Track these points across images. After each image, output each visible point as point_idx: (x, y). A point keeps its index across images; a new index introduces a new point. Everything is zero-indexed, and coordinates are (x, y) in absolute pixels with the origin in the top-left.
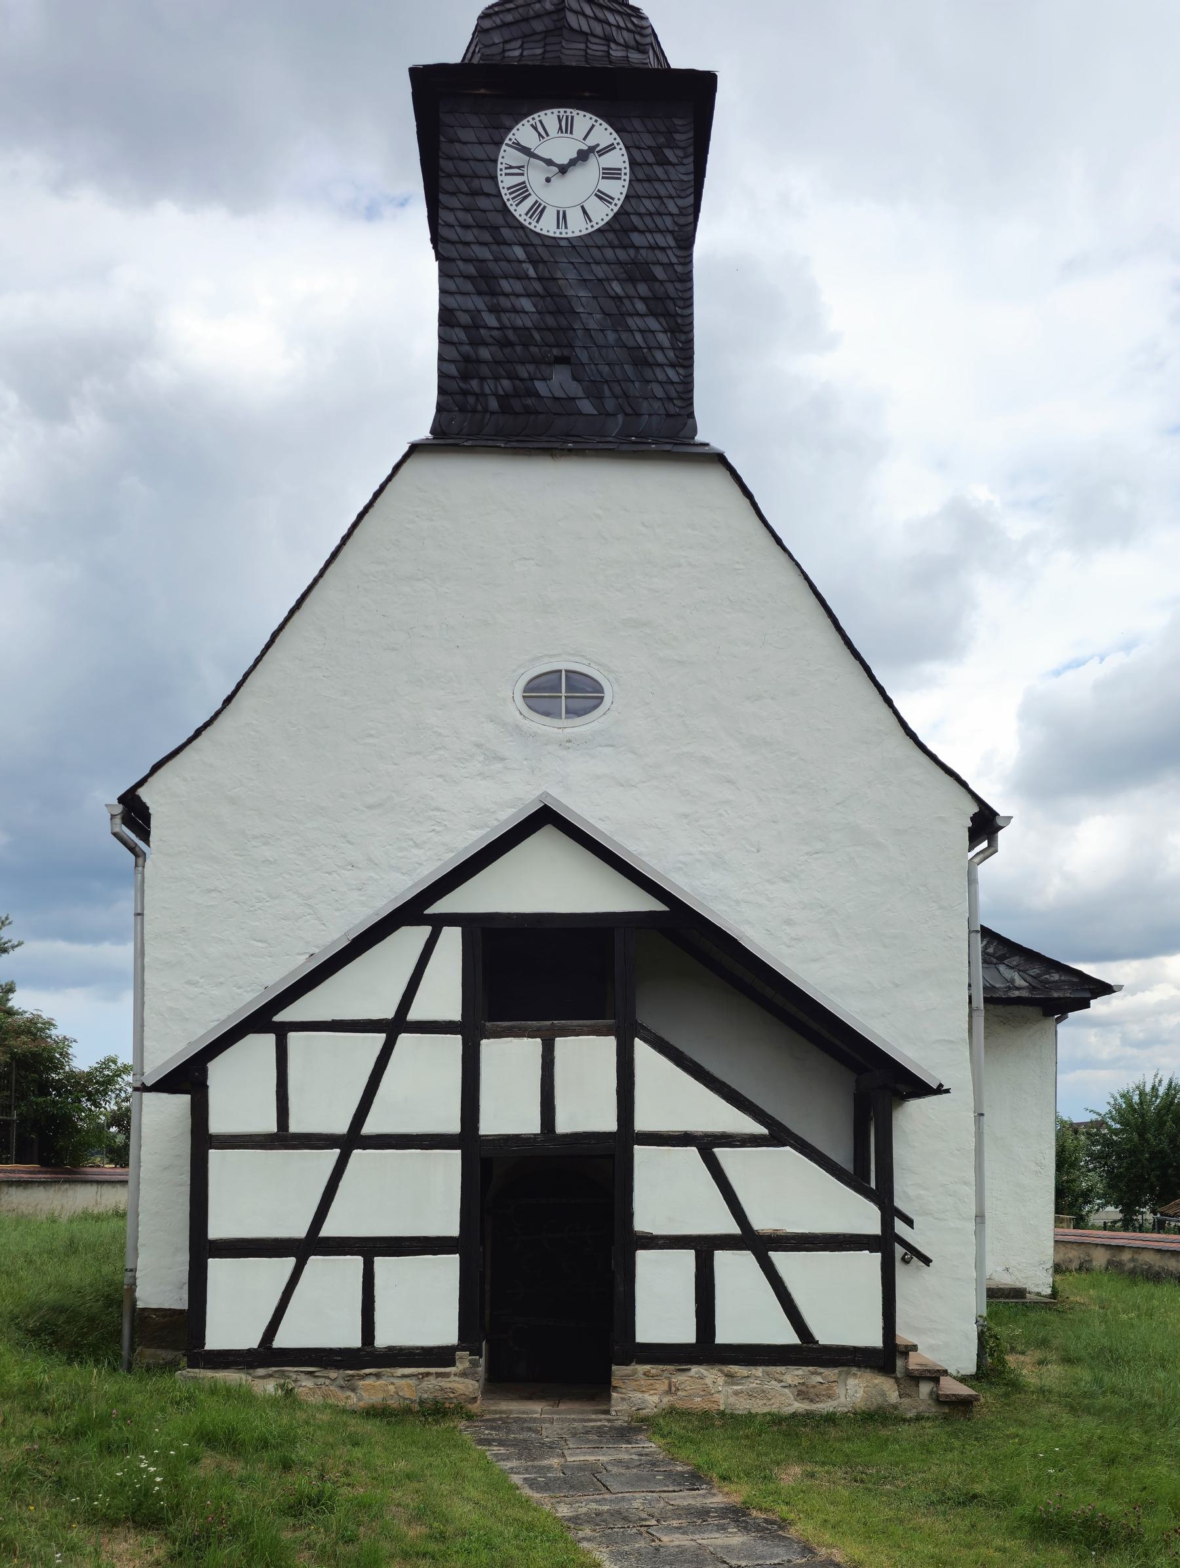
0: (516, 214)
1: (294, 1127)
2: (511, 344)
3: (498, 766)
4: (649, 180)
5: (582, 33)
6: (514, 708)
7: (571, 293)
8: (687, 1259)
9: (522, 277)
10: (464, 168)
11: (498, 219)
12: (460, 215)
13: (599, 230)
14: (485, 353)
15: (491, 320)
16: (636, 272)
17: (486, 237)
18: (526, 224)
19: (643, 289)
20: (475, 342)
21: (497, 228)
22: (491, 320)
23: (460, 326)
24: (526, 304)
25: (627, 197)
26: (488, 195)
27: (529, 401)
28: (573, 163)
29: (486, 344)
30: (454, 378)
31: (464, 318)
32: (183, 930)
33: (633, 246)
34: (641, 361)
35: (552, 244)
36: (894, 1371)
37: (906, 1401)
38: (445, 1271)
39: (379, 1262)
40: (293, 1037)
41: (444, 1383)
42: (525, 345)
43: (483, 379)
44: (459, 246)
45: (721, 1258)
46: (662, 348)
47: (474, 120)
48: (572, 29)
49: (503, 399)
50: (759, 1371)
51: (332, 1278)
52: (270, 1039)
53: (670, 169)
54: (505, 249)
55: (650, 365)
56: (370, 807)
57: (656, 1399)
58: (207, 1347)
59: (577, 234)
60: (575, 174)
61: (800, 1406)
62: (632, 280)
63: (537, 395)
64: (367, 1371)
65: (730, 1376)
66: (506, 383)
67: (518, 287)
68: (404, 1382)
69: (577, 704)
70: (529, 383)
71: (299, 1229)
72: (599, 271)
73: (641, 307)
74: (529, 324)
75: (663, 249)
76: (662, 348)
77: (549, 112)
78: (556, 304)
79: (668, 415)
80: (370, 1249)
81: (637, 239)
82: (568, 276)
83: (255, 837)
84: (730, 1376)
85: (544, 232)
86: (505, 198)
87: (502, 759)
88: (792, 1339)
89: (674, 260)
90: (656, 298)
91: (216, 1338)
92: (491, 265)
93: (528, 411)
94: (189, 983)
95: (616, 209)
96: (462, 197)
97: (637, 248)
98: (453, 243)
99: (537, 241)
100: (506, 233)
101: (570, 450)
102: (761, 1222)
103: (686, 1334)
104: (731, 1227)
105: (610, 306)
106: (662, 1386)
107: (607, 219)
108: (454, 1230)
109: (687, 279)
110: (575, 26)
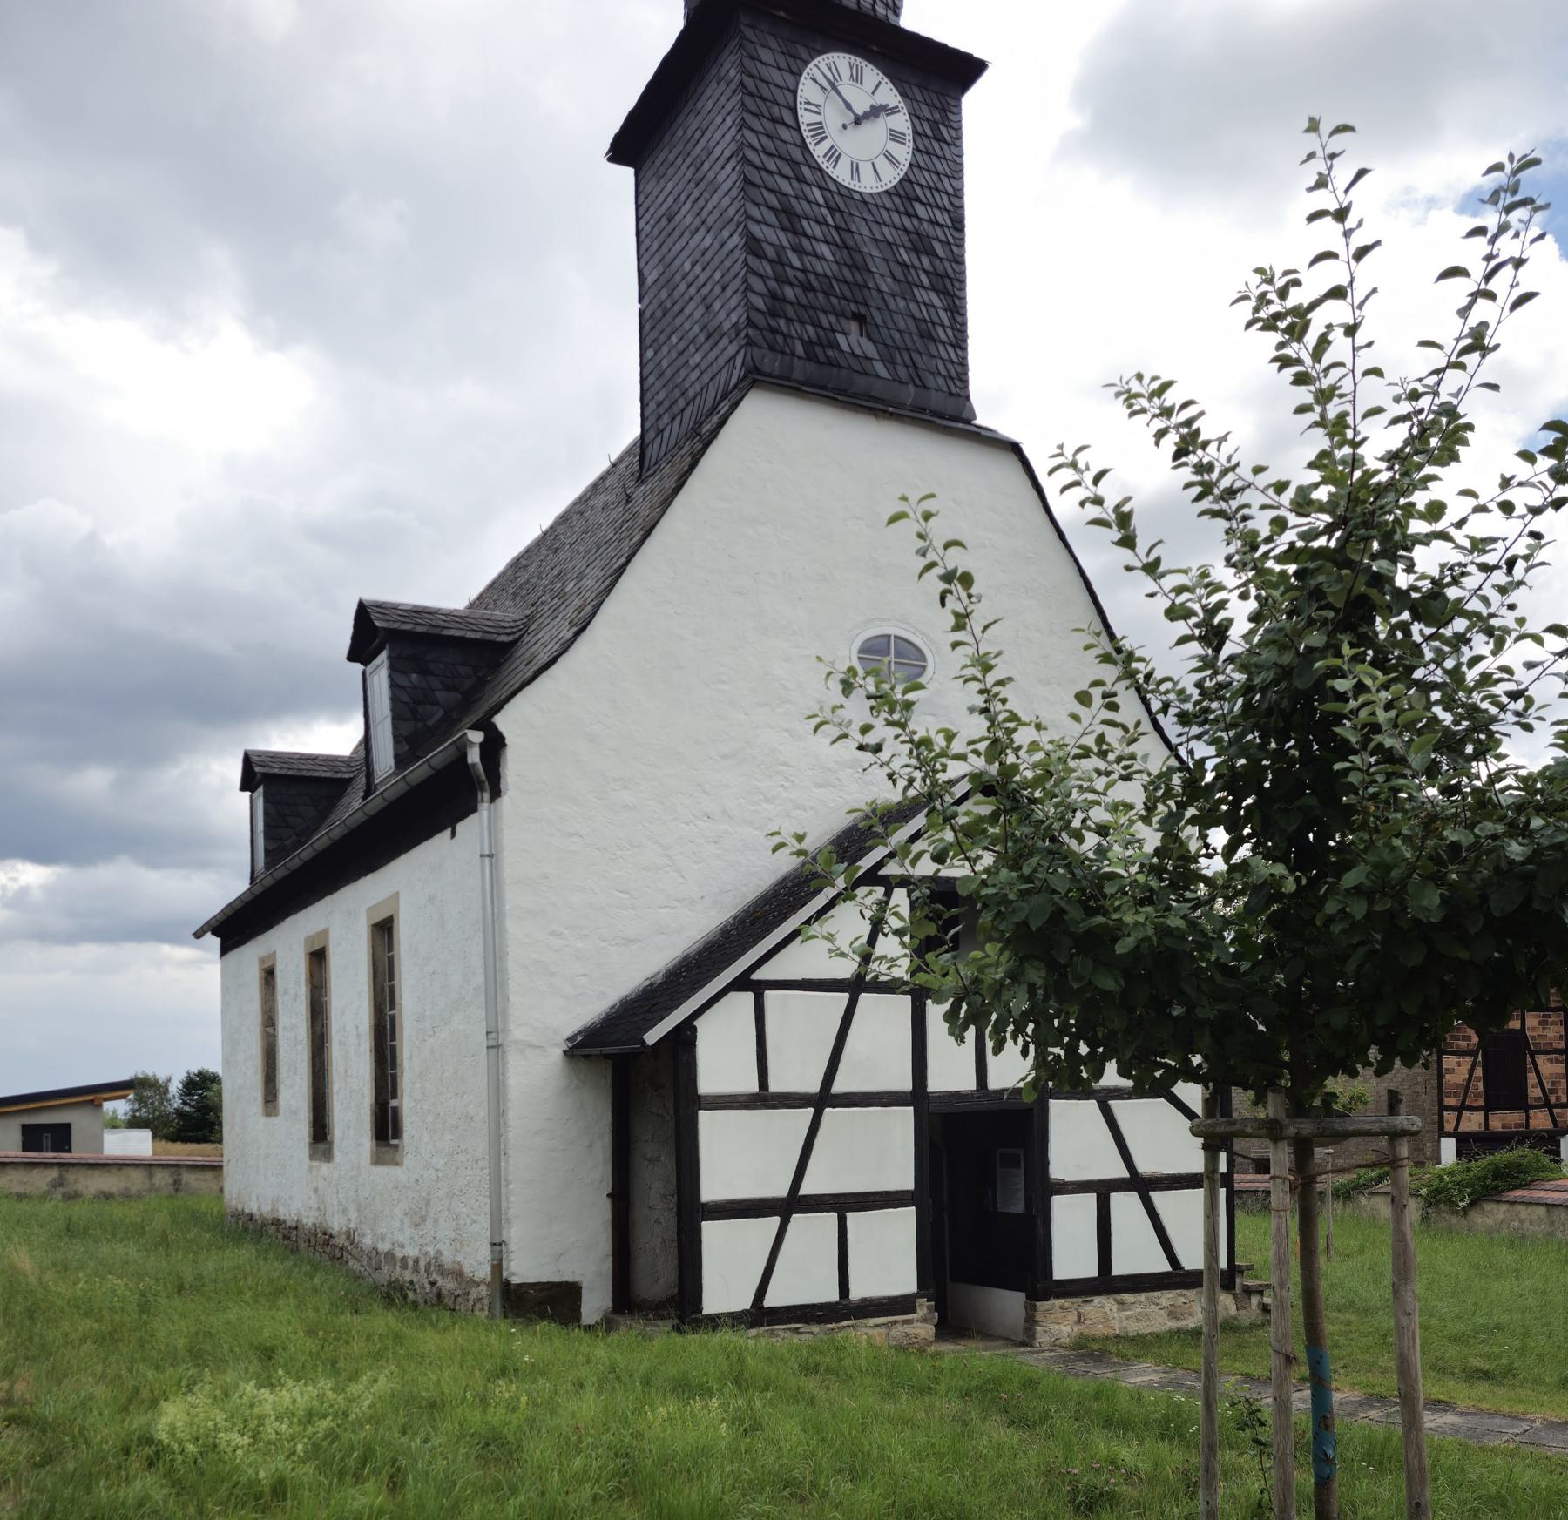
0: (815, 154)
1: (774, 1087)
2: (813, 290)
7: (865, 250)
8: (1091, 1199)
9: (822, 222)
11: (797, 154)
12: (764, 139)
13: (887, 192)
14: (789, 293)
15: (795, 260)
17: (787, 170)
19: (925, 261)
21: (798, 164)
22: (795, 260)
24: (824, 250)
26: (788, 126)
27: (830, 353)
28: (867, 116)
29: (791, 285)
31: (770, 252)
35: (847, 194)
36: (577, 1317)
37: (1242, 1312)
39: (851, 1217)
40: (770, 996)
41: (908, 1329)
42: (826, 294)
44: (764, 174)
45: (1116, 1199)
46: (943, 326)
47: (772, 43)
49: (808, 344)
50: (1142, 1297)
52: (749, 997)
54: (806, 188)
55: (934, 340)
56: (725, 757)
57: (1068, 1329)
58: (705, 1312)
59: (868, 190)
61: (1173, 1324)
62: (916, 250)
63: (840, 350)
64: (845, 1323)
65: (1121, 1303)
66: (810, 329)
67: (818, 232)
68: (876, 1331)
70: (830, 334)
74: (829, 273)
75: (941, 226)
76: (943, 326)
79: (951, 394)
80: (843, 1204)
84: (1121, 1303)
86: (805, 134)
88: (1165, 1267)
90: (937, 274)
91: (713, 1303)
92: (793, 201)
93: (831, 363)
94: (553, 933)
97: (920, 219)
99: (833, 188)
100: (806, 171)
101: (892, 414)
102: (1145, 1167)
103: (1091, 1270)
104: (1124, 1173)
106: (1073, 1317)
107: (895, 182)
108: (909, 1185)
109: (959, 261)
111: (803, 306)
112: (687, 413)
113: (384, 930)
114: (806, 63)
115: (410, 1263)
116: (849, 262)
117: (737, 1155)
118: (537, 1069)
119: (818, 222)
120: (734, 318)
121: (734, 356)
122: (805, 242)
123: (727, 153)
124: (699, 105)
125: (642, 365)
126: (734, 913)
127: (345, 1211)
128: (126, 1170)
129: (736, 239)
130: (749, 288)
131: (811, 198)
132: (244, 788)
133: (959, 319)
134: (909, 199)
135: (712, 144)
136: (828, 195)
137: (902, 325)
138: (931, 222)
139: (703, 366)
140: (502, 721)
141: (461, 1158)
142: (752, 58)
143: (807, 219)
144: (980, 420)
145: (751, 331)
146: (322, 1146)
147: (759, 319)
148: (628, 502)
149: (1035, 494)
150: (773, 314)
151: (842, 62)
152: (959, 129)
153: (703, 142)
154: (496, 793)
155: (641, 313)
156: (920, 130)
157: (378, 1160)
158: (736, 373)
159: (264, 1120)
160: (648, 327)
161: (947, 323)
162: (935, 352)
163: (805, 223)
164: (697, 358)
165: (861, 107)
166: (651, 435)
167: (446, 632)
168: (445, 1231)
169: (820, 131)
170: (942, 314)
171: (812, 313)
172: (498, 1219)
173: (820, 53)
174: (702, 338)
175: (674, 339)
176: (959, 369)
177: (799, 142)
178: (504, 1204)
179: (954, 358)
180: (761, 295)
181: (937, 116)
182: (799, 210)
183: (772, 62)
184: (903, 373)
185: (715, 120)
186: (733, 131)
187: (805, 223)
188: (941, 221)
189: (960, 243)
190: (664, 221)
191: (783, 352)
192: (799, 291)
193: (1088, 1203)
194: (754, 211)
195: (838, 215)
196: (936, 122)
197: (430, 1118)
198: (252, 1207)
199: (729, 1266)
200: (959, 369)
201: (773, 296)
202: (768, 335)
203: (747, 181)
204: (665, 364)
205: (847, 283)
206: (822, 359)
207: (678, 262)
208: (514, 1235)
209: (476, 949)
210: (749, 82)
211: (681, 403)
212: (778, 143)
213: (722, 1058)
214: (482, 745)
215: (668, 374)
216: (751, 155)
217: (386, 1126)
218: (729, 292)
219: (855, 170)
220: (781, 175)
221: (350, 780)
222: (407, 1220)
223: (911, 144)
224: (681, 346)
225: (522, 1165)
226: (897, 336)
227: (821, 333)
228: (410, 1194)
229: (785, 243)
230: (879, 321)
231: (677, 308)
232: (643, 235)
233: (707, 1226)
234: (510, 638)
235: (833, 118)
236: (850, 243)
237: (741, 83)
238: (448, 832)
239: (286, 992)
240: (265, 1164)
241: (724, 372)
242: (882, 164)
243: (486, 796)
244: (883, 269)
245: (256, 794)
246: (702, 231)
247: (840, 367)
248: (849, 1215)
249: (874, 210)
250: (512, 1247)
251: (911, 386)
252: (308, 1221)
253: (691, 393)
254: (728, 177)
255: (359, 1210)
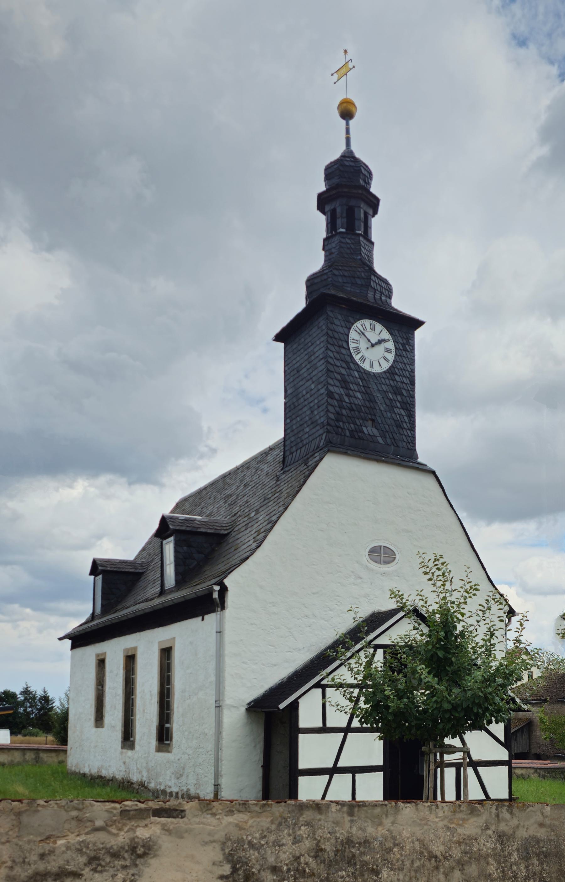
0: (355, 359)
1: (329, 725)
2: (354, 410)
3: (360, 580)
4: (401, 356)
5: (374, 289)
6: (365, 559)
7: (375, 394)
9: (358, 384)
10: (336, 335)
11: (348, 359)
12: (335, 354)
13: (384, 372)
14: (344, 412)
16: (397, 391)
17: (344, 365)
18: (359, 363)
20: (341, 407)
21: (348, 362)
23: (335, 399)
24: (359, 395)
25: (394, 361)
26: (345, 348)
27: (360, 434)
28: (376, 344)
29: (345, 409)
30: (333, 420)
31: (337, 397)
32: (241, 640)
33: (396, 380)
34: (399, 426)
35: (368, 373)
38: (379, 777)
39: (357, 776)
42: (359, 412)
43: (344, 422)
44: (335, 367)
46: (406, 423)
48: (371, 287)
49: (351, 431)
51: (342, 782)
52: (320, 691)
53: (407, 353)
54: (351, 372)
56: (313, 593)
59: (377, 371)
60: (377, 348)
62: (395, 394)
63: (364, 433)
66: (352, 426)
69: (387, 559)
70: (360, 427)
71: (330, 765)
72: (385, 388)
73: (398, 405)
74: (360, 404)
75: (406, 384)
76: (406, 423)
77: (367, 320)
78: (370, 398)
79: (408, 449)
80: (354, 771)
81: (397, 378)
82: (373, 387)
83: (270, 603)
85: (365, 368)
86: (352, 351)
87: (361, 578)
89: (409, 389)
90: (403, 402)
92: (347, 377)
93: (360, 438)
94: (243, 662)
95: (390, 365)
96: (336, 347)
97: (397, 381)
98: (332, 365)
99: (362, 371)
100: (352, 365)
102: (475, 757)
105: (388, 402)
107: (387, 368)
109: (413, 397)
110: (373, 286)
111: (350, 417)
112: (303, 449)
113: (166, 653)
114: (353, 324)
115: (174, 794)
116: (368, 399)
117: (313, 751)
118: (234, 717)
119: (356, 384)
120: (322, 420)
121: (322, 434)
122: (351, 392)
123: (321, 357)
124: (311, 333)
125: (285, 424)
126: (316, 654)
127: (140, 772)
128: (12, 752)
129: (322, 391)
130: (328, 411)
131: (353, 375)
132: (91, 574)
133: (412, 419)
134: (393, 374)
135: (315, 350)
136: (360, 373)
137: (389, 423)
138: (402, 382)
139: (310, 433)
140: (227, 582)
141: (200, 750)
142: (331, 323)
143: (352, 383)
144: (420, 460)
145: (329, 427)
146: (128, 743)
147: (332, 422)
148: (277, 481)
149: (441, 490)
150: (338, 420)
151: (367, 323)
152: (413, 346)
153: (311, 348)
154: (223, 608)
155: (285, 404)
156: (398, 347)
157: (159, 750)
158: (322, 441)
159: (95, 729)
160: (288, 410)
161: (407, 421)
162: (402, 433)
163: (351, 385)
164: (307, 430)
165: (374, 341)
166: (288, 453)
167: (199, 530)
168: (192, 780)
169: (358, 350)
170: (406, 418)
171: (353, 419)
172: (217, 775)
173: (359, 320)
174: (309, 423)
175: (298, 419)
176: (412, 439)
177: (349, 354)
178: (220, 769)
179: (410, 435)
180: (333, 413)
181: (405, 341)
182: (349, 380)
183: (339, 324)
184: (389, 441)
185: (316, 336)
186: (323, 349)
187: (351, 385)
188: (405, 381)
189: (413, 390)
190: (295, 371)
191: (341, 435)
192: (348, 411)
193: (453, 770)
194: (331, 381)
195: (364, 381)
196: (404, 344)
197: (186, 733)
198: (86, 770)
199: (309, 789)
200: (412, 439)
201: (338, 413)
202: (335, 428)
203: (328, 370)
204: (294, 427)
205: (367, 407)
206: (357, 437)
207: (300, 389)
208: (224, 782)
209: (212, 665)
210: (330, 332)
211: (300, 445)
212: (341, 355)
213: (309, 712)
214: (219, 591)
215: (296, 431)
216: (330, 360)
217: (164, 736)
218: (321, 409)
219: (371, 364)
220: (342, 367)
221: (143, 573)
222: (173, 776)
223: (394, 353)
224: (301, 423)
225: (227, 754)
226: (387, 427)
227: (356, 426)
228: (175, 765)
229: (343, 393)
230: (380, 421)
231: (300, 407)
232: (287, 374)
233: (300, 778)
234: (226, 532)
235: (363, 345)
236: (369, 392)
237: (327, 332)
238: (200, 618)
239: (111, 672)
240: (93, 748)
241: (318, 439)
242: (383, 362)
243: (219, 609)
244: (382, 401)
245: (97, 578)
246: (310, 382)
247: (364, 439)
248: (357, 775)
249: (379, 379)
250: (222, 786)
251: (392, 446)
252: (119, 776)
253: (305, 442)
254: (321, 366)
255: (148, 771)
